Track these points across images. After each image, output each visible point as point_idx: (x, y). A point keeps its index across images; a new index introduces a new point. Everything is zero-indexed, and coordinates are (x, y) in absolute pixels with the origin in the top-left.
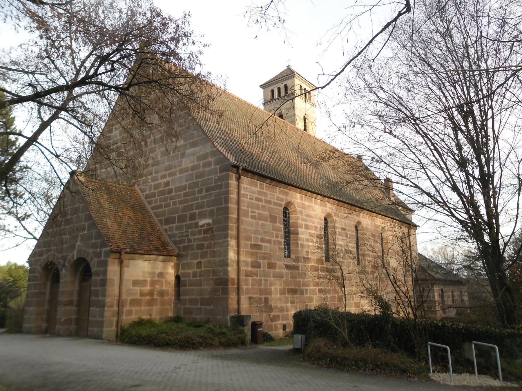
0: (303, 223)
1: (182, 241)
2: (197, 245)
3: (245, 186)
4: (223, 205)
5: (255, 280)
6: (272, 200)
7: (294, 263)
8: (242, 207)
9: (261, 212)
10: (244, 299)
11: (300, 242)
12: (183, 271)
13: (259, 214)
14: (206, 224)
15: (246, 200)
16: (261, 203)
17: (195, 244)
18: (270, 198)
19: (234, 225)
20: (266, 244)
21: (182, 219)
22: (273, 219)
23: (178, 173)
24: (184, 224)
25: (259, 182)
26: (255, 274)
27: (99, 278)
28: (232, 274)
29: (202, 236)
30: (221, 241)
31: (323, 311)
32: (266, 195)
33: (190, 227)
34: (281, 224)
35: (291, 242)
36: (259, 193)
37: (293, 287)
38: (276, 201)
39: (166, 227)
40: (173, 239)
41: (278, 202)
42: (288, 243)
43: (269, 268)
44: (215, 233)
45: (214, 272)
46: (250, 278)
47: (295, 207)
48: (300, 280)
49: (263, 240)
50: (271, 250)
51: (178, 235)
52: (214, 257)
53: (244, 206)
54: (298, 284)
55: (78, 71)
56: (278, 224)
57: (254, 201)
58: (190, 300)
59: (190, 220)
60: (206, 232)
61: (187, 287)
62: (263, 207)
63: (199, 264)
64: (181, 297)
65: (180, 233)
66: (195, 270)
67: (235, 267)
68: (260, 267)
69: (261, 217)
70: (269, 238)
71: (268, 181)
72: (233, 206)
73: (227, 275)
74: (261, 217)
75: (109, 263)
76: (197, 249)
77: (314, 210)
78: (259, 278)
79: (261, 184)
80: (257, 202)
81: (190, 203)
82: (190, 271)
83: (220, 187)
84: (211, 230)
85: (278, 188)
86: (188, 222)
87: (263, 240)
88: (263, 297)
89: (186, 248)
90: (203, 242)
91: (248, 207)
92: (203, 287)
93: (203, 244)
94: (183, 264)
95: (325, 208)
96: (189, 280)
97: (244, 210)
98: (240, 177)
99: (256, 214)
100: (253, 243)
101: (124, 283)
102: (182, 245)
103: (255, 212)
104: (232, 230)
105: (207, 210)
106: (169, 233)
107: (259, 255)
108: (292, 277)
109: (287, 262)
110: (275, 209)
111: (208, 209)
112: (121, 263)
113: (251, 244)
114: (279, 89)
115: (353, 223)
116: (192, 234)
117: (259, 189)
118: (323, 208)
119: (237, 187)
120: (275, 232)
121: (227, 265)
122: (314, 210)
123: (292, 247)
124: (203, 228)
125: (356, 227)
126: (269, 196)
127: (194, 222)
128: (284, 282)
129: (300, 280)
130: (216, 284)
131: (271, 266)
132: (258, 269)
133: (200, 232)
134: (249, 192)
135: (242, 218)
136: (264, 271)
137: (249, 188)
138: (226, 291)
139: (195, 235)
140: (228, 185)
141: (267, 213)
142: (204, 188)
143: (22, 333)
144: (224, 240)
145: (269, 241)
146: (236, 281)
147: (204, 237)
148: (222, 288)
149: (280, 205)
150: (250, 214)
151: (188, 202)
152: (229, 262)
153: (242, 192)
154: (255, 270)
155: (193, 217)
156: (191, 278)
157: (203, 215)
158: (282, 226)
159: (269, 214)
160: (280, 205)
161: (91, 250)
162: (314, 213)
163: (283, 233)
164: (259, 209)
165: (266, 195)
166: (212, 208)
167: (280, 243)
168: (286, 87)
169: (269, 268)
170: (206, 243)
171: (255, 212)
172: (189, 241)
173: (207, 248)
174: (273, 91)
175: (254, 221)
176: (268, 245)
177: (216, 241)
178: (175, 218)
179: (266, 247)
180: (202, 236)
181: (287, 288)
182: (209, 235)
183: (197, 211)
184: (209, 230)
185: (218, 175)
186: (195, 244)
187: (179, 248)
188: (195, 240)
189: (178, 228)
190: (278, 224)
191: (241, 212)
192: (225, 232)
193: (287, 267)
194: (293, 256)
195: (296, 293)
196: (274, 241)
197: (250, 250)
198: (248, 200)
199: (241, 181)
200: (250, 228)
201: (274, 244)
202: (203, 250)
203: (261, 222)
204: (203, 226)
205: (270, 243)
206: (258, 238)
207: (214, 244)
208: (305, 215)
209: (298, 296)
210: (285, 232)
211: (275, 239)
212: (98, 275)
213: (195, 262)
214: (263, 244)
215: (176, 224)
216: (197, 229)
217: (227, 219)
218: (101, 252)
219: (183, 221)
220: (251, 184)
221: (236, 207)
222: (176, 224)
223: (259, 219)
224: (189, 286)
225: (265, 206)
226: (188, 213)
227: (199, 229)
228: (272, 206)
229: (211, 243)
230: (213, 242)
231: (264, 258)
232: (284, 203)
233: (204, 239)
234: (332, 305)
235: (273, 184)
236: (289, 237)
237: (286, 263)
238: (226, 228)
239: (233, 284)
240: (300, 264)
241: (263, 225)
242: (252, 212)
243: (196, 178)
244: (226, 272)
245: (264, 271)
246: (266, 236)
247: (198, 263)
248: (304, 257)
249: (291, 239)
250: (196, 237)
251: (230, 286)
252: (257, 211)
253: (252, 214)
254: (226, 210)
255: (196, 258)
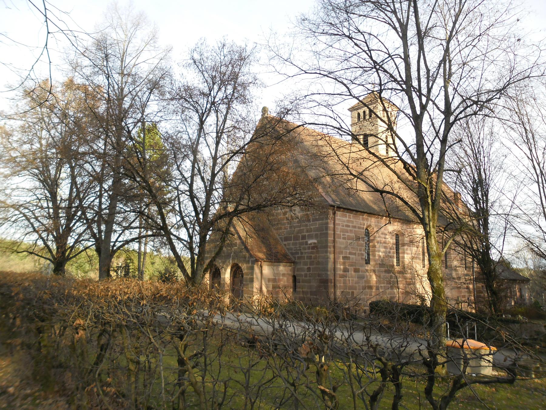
1: (297, 253)
3: (339, 217)
4: (324, 232)
8: (336, 233)
9: (349, 234)
13: (348, 235)
15: (339, 227)
16: (349, 229)
21: (296, 238)
24: (298, 242)
25: (348, 214)
27: (248, 277)
28: (330, 274)
29: (310, 250)
30: (323, 255)
32: (352, 222)
33: (301, 244)
36: (348, 221)
39: (286, 243)
40: (290, 251)
49: (350, 253)
50: (356, 260)
57: (345, 228)
59: (302, 239)
60: (313, 248)
62: (351, 231)
67: (333, 272)
70: (354, 252)
71: (354, 212)
72: (331, 232)
79: (349, 215)
80: (346, 228)
82: (303, 273)
84: (316, 247)
86: (301, 241)
87: (350, 253)
88: (350, 291)
89: (299, 258)
93: (311, 256)
97: (338, 234)
98: (335, 213)
102: (296, 256)
106: (287, 247)
114: (364, 112)
120: (359, 248)
121: (327, 270)
133: (309, 248)
137: (342, 218)
138: (326, 288)
145: (355, 254)
146: (333, 281)
153: (337, 222)
154: (345, 273)
157: (310, 237)
165: (352, 222)
170: (313, 255)
172: (302, 253)
173: (314, 259)
174: (359, 114)
175: (344, 241)
178: (291, 237)
179: (353, 258)
180: (310, 250)
182: (315, 251)
183: (307, 234)
184: (315, 247)
187: (295, 258)
188: (305, 253)
189: (293, 244)
199: (336, 215)
201: (358, 255)
204: (311, 244)
212: (248, 275)
219: (297, 240)
226: (300, 235)
228: (357, 229)
231: (351, 265)
233: (312, 253)
238: (326, 247)
239: (331, 283)
244: (327, 275)
247: (308, 268)
250: (307, 251)
251: (329, 284)
252: (347, 234)
254: (326, 235)
255: (306, 265)
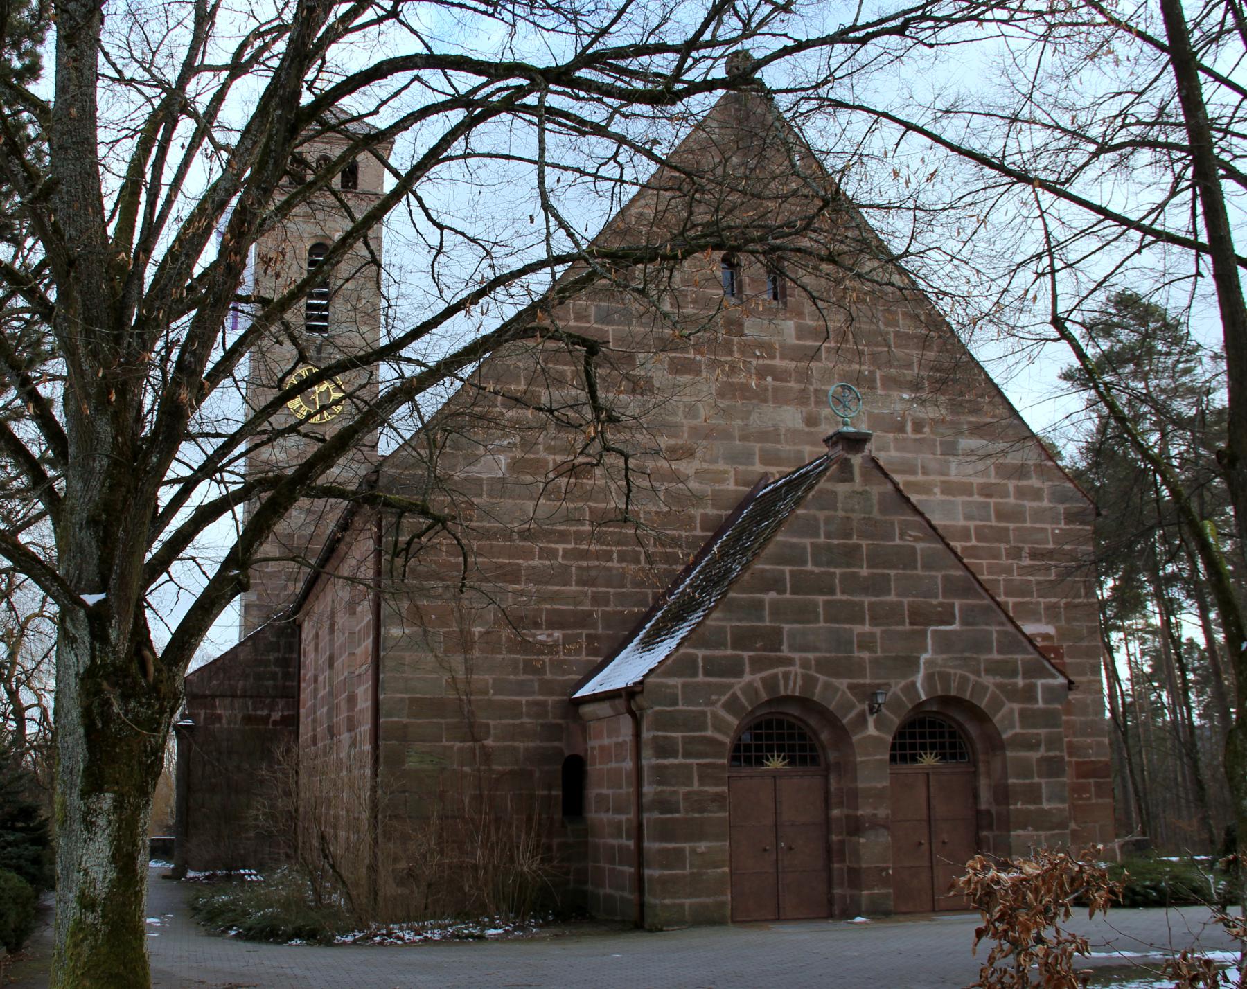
23: (937, 490)
44: (1067, 660)
55: (1014, 183)
142: (1027, 547)
143: (655, 929)
144: (1092, 678)
148: (1097, 784)
161: (989, 681)
185: (1063, 526)
192: (1092, 661)
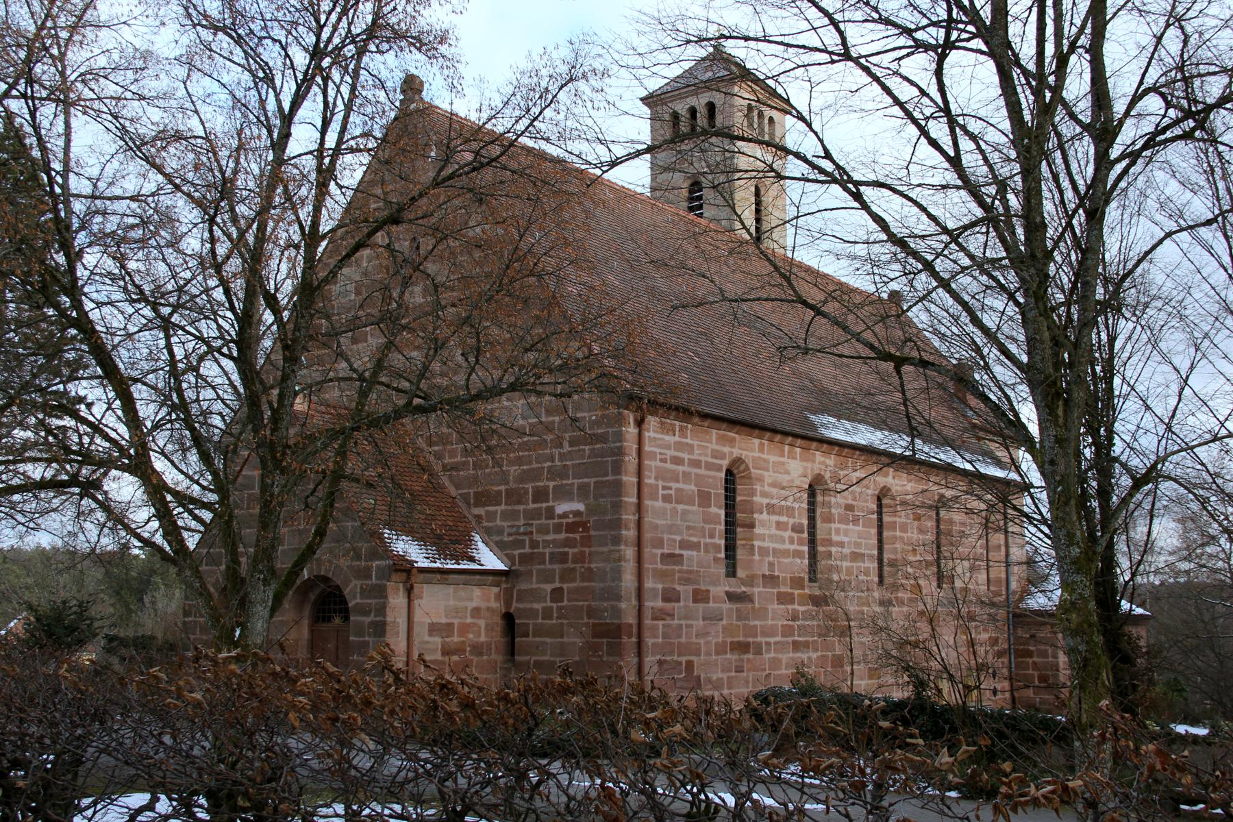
0: (765, 501)
2: (551, 554)
3: (652, 434)
4: (610, 478)
5: (669, 626)
6: (703, 459)
7: (744, 589)
8: (647, 481)
9: (680, 485)
10: (650, 660)
11: (756, 543)
12: (521, 606)
13: (677, 490)
14: (572, 512)
15: (653, 463)
16: (681, 468)
17: (547, 551)
18: (700, 454)
19: (631, 517)
20: (690, 553)
21: (515, 496)
22: (704, 499)
24: (521, 507)
25: (677, 423)
26: (669, 615)
30: (605, 549)
31: (806, 688)
34: (720, 508)
35: (738, 542)
36: (679, 446)
37: (741, 639)
38: (710, 460)
41: (715, 461)
42: (730, 548)
43: (695, 601)
44: (592, 533)
45: (591, 612)
46: (661, 623)
47: (747, 468)
48: (757, 623)
49: (684, 545)
50: (700, 565)
51: (507, 531)
52: (590, 580)
53: (650, 478)
54: (752, 631)
56: (713, 510)
57: (669, 466)
58: (538, 664)
59: (534, 502)
60: (571, 528)
61: (530, 638)
63: (557, 594)
64: (517, 658)
65: (512, 526)
66: (549, 604)
68: (678, 601)
69: (681, 498)
70: (695, 539)
73: (619, 617)
74: (681, 498)
75: (390, 591)
76: (551, 562)
77: (787, 472)
78: (676, 622)
79: (681, 429)
80: (674, 467)
81: (535, 465)
82: (538, 606)
83: (603, 438)
84: (584, 525)
85: (714, 431)
86: (531, 506)
87: (684, 545)
90: (566, 549)
91: (656, 478)
92: (565, 640)
93: (567, 553)
94: (519, 591)
95: (809, 465)
96: (535, 624)
99: (672, 492)
100: (666, 551)
101: (416, 630)
102: (516, 552)
103: (670, 488)
104: (628, 529)
105: (573, 484)
107: (677, 575)
108: (739, 618)
109: (730, 586)
110: (709, 477)
111: (576, 481)
112: (409, 591)
113: (662, 555)
115: (872, 492)
116: (539, 531)
117: (677, 438)
118: (804, 464)
119: (636, 439)
120: (707, 526)
122: (787, 472)
123: (740, 554)
124: (564, 521)
125: (879, 499)
126: (696, 452)
127: (544, 505)
128: (725, 629)
129: (757, 623)
130: (596, 635)
131: (700, 597)
132: (676, 605)
134: (659, 446)
135: (647, 502)
136: (686, 607)
139: (548, 533)
140: (619, 437)
141: (693, 487)
145: (695, 546)
146: (635, 630)
147: (567, 539)
149: (719, 468)
150: (661, 492)
151: (530, 463)
152: (623, 593)
154: (669, 605)
155: (540, 495)
156: (540, 621)
157: (564, 494)
158: (722, 512)
159: (696, 489)
160: (719, 468)
162: (787, 477)
163: (723, 527)
164: (677, 481)
166: (585, 480)
167: (717, 547)
168: (711, 107)
169: (695, 601)
171: (670, 488)
172: (534, 544)
175: (668, 506)
176: (695, 553)
177: (593, 549)
178: (500, 492)
179: (690, 559)
180: (563, 535)
181: (729, 640)
182: (577, 536)
184: (577, 525)
186: (547, 551)
189: (506, 516)
190: (713, 510)
191: (645, 490)
193: (731, 597)
194: (741, 573)
195: (748, 652)
196: (706, 544)
197: (660, 566)
198: (658, 463)
199: (645, 426)
200: (660, 522)
201: (707, 551)
202: (566, 566)
203: (680, 507)
204: (565, 515)
205: (699, 551)
206: (674, 541)
207: (590, 554)
208: (769, 485)
209: (751, 656)
210: (727, 523)
211: (708, 540)
212: (366, 613)
213: (548, 587)
214: (683, 552)
215: (503, 507)
216: (551, 522)
217: (618, 506)
218: (369, 569)
219: (519, 502)
220: (665, 429)
221: (635, 480)
222: (503, 507)
223: (677, 502)
224: (534, 636)
225: (690, 473)
226: (529, 486)
227: (556, 521)
228: (703, 472)
229: (583, 553)
230: (587, 550)
231: (687, 581)
232: (725, 463)
233: (568, 543)
234: (823, 678)
235: (706, 424)
236: (734, 532)
237: (727, 589)
239: (630, 637)
240: (756, 590)
241: (684, 512)
242: (664, 488)
243: (681, 548)
245: (686, 607)
246: (691, 535)
247: (554, 590)
248: (764, 576)
249: (739, 536)
250: (550, 537)
252: (674, 485)
253: (665, 492)
254: (617, 488)
